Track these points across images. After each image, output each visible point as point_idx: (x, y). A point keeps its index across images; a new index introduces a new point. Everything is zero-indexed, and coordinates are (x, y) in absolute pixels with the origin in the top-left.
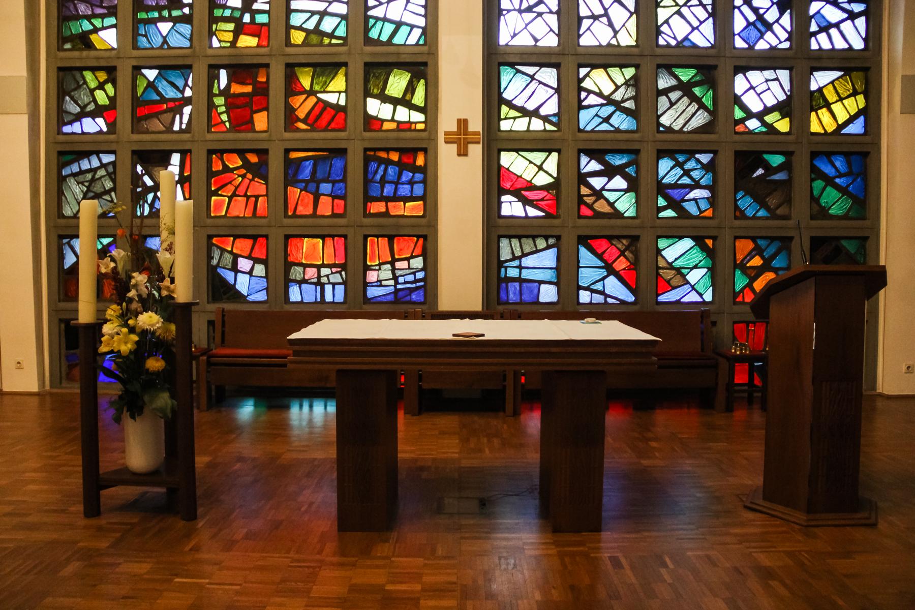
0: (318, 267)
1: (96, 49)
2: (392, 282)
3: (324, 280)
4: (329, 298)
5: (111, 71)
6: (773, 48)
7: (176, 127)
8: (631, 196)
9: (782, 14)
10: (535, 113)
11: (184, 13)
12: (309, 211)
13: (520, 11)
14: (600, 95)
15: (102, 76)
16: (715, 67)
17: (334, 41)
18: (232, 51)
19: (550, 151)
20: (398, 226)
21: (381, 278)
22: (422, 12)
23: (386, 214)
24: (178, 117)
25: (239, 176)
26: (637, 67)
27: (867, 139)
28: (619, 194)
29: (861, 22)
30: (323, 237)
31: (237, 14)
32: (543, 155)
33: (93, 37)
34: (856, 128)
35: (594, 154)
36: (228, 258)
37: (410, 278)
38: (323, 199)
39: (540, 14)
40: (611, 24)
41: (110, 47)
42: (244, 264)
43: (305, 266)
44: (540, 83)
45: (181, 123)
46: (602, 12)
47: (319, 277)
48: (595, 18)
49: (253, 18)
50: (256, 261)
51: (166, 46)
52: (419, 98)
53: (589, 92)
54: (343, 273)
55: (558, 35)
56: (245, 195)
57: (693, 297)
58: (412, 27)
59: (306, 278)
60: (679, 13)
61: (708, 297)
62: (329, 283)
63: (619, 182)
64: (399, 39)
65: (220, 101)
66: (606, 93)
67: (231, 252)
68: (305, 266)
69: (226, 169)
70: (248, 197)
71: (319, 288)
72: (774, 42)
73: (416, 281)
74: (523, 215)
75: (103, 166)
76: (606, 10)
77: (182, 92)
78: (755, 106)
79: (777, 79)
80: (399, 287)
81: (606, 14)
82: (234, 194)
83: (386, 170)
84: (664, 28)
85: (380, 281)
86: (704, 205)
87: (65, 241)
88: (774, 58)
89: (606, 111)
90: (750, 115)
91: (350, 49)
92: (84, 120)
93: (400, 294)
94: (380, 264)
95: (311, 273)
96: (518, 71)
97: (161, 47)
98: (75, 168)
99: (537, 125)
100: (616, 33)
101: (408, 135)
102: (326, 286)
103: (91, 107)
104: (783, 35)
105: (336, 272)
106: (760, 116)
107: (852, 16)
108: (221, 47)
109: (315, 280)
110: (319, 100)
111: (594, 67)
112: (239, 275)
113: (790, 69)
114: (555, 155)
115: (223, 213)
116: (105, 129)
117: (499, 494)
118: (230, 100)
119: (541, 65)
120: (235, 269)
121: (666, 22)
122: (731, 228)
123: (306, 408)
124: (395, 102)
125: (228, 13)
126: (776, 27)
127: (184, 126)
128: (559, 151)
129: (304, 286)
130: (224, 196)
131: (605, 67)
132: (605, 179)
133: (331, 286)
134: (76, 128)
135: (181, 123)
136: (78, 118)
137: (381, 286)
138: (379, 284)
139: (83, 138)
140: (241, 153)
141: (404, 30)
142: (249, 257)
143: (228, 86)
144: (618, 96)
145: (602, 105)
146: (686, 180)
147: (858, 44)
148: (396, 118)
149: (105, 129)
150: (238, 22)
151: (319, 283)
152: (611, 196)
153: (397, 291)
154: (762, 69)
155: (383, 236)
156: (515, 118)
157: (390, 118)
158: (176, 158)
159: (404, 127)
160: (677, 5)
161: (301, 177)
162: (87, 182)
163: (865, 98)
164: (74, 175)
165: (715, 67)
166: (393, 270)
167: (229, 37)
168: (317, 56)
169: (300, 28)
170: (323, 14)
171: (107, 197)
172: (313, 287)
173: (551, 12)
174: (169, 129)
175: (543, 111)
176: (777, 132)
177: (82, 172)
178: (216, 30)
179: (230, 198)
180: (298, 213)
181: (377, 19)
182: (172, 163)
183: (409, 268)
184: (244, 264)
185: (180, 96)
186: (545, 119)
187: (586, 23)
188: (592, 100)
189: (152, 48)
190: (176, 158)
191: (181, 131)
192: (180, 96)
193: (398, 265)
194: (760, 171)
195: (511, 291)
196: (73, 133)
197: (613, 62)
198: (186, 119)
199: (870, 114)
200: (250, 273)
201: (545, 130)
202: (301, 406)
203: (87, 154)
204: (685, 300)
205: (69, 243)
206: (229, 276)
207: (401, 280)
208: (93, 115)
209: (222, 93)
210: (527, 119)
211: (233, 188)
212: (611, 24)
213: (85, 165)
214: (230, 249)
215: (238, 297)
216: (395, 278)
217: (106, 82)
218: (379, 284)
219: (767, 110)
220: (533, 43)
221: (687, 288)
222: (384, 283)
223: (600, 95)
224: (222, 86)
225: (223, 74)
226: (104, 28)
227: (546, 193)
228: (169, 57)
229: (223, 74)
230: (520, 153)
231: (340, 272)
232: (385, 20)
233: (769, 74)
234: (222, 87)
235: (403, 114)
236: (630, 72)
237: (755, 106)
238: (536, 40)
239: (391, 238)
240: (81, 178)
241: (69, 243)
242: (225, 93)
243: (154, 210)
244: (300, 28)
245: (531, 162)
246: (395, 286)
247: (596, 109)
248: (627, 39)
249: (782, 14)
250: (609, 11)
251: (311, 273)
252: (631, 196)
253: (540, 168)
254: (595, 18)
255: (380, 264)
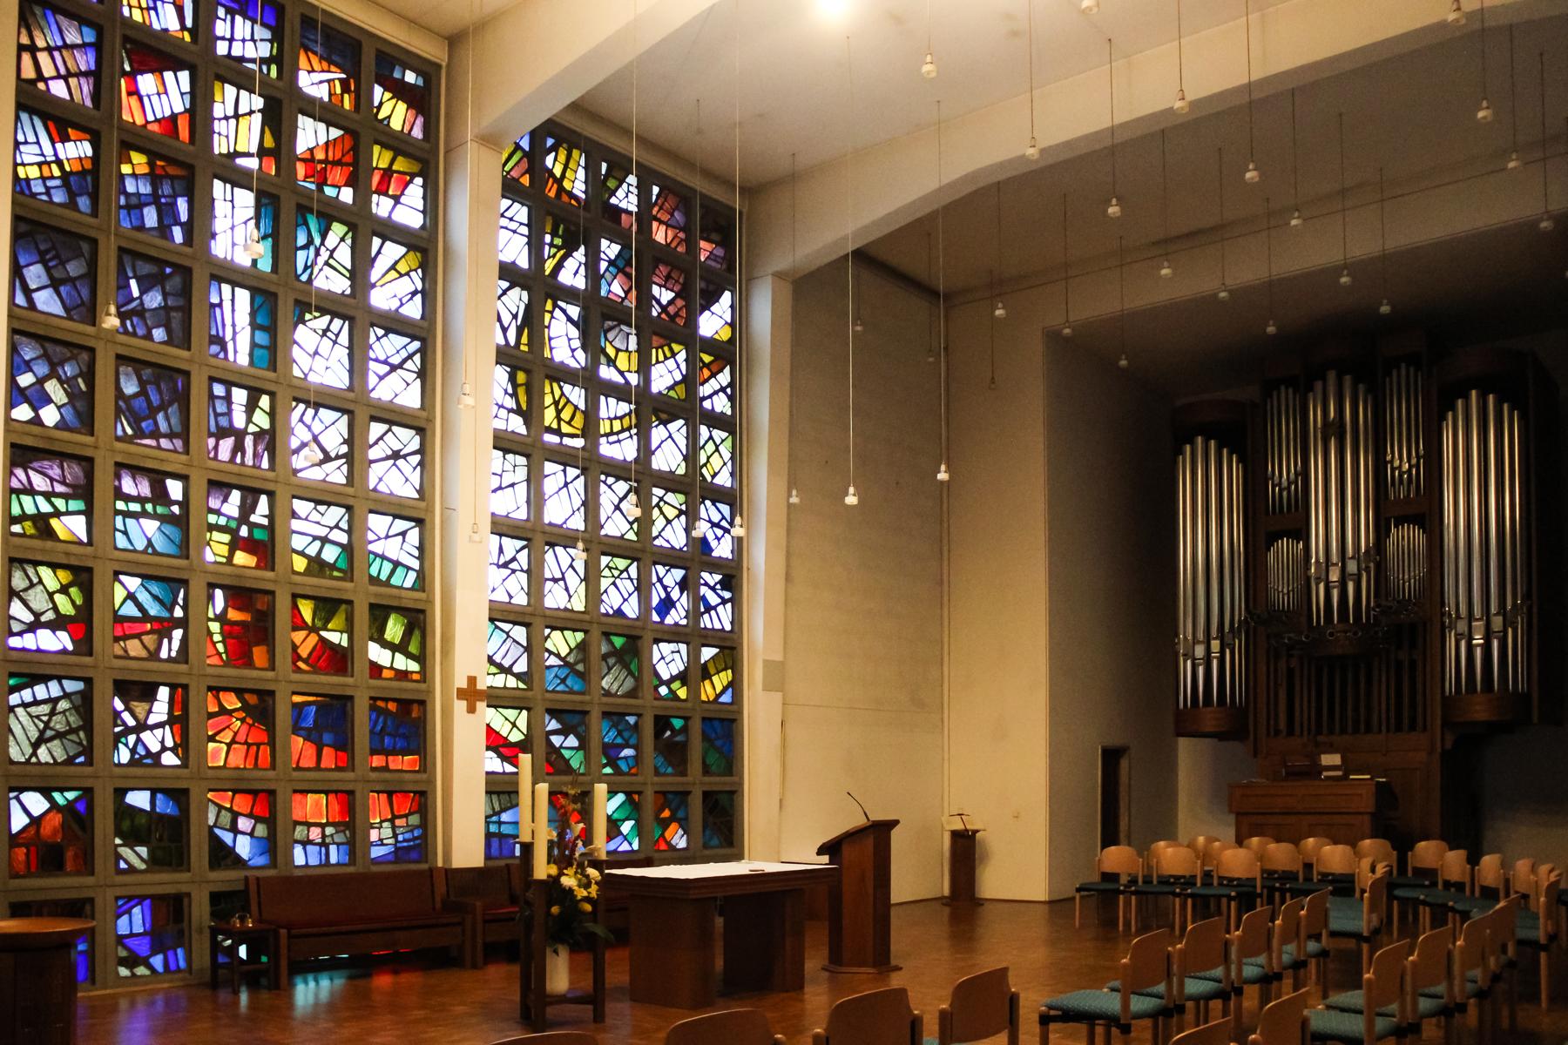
0: (323, 826)
1: (59, 540)
2: (391, 841)
3: (328, 840)
4: (333, 859)
5: (77, 571)
6: (676, 624)
7: (164, 654)
8: (580, 754)
9: (682, 593)
10: (507, 671)
11: (173, 513)
12: (312, 764)
13: (499, 566)
14: (558, 656)
15: (64, 576)
16: (639, 637)
17: (336, 574)
18: (228, 569)
19: (521, 709)
20: (401, 781)
21: (382, 837)
22: (416, 553)
23: (386, 769)
24: (166, 641)
25: (237, 719)
26: (586, 632)
27: (734, 708)
28: (573, 752)
29: (729, 606)
30: (327, 793)
31: (233, 524)
32: (516, 712)
33: (54, 522)
34: (726, 698)
35: (553, 713)
36: (226, 818)
37: (408, 836)
38: (326, 751)
39: (514, 571)
40: (567, 589)
41: (75, 539)
42: (244, 824)
43: (309, 825)
44: (514, 641)
45: (170, 650)
46: (560, 576)
47: (324, 836)
48: (555, 580)
49: (250, 532)
50: (258, 820)
51: (150, 550)
52: (413, 648)
53: (551, 653)
54: (347, 832)
55: (527, 594)
56: (246, 743)
57: (625, 847)
58: (409, 568)
59: (311, 838)
60: (614, 584)
61: (636, 846)
62: (334, 843)
63: (572, 741)
64: (395, 581)
65: (215, 627)
66: (563, 655)
67: (230, 810)
68: (309, 825)
69: (223, 711)
70: (249, 745)
71: (323, 849)
72: (677, 619)
73: (415, 838)
74: (501, 771)
75: (66, 696)
76: (563, 574)
77: (171, 610)
78: (665, 676)
79: (678, 652)
80: (399, 845)
81: (563, 579)
82: (233, 741)
83: (385, 722)
84: (604, 597)
85: (381, 840)
86: (631, 762)
87: (12, 795)
88: (678, 634)
89: (566, 671)
90: (662, 682)
91: (355, 587)
92: (39, 632)
93: (400, 853)
94: (382, 822)
95: (315, 834)
96: (497, 627)
97: (145, 552)
98: (27, 695)
99: (512, 682)
100: (570, 597)
101: (405, 684)
102: (331, 846)
103: (50, 616)
104: (683, 614)
105: (341, 831)
106: (668, 683)
107: (724, 602)
108: (216, 562)
109: (320, 841)
110: (323, 640)
111: (554, 628)
112: (240, 837)
113: (688, 644)
114: (525, 713)
115: (222, 764)
116: (70, 647)
117: (552, 392)
118: (226, 627)
119: (515, 623)
120: (235, 830)
121: (606, 591)
122: (652, 784)
123: (312, 984)
124: (394, 648)
125: (222, 521)
126: (678, 605)
127: (173, 654)
128: (528, 709)
129: (309, 848)
130: (221, 742)
131: (562, 629)
132: (562, 738)
133: (335, 846)
134: (28, 641)
135: (170, 650)
136: (32, 628)
137: (383, 845)
138: (381, 843)
139: (38, 656)
140: (239, 692)
141: (400, 571)
142: (249, 816)
143: (225, 611)
144: (571, 659)
145: (559, 666)
146: (619, 740)
147: (728, 627)
148: (395, 666)
149: (70, 647)
150: (234, 533)
151: (324, 844)
152: (567, 754)
153: (397, 849)
154: (669, 642)
155: (383, 792)
156: (494, 674)
157: (389, 666)
158: (163, 693)
159: (403, 675)
160: (613, 576)
161: (303, 725)
162: (45, 715)
163: (733, 672)
164: (25, 705)
165: (639, 637)
166: (394, 828)
167: (224, 550)
168: (150, 354)
169: (302, 553)
170: (325, 540)
171: (73, 737)
172: (318, 848)
173: (522, 570)
174: (154, 655)
175: (516, 669)
176: (677, 698)
177: (36, 703)
178: (210, 539)
179: (229, 745)
180: (301, 765)
181: (376, 555)
182: (158, 698)
183: (408, 825)
184: (244, 824)
185: (165, 614)
186: (518, 676)
187: (549, 585)
188: (553, 661)
189: (135, 551)
190: (163, 693)
191: (170, 660)
192: (165, 614)
193: (398, 822)
194: (668, 733)
195: (139, 945)
196: (24, 649)
197: (569, 626)
198: (176, 644)
199: (735, 685)
200: (251, 834)
201: (518, 688)
202: (306, 983)
203: (44, 679)
204: (620, 849)
205: (17, 798)
206: (227, 837)
207: (400, 838)
208: (54, 626)
209: (217, 618)
210: (504, 675)
211: (232, 734)
212: (567, 589)
213: (41, 691)
214: (228, 806)
215: (238, 861)
216: (395, 836)
217: (71, 585)
218: (381, 843)
219: (673, 679)
220: (506, 599)
221: (619, 839)
222: (385, 842)
223: (558, 656)
224: (218, 611)
225: (219, 594)
226: (68, 513)
227: (603, 280)
228: (148, 564)
229: (219, 594)
230: (500, 709)
231: (344, 832)
232: (383, 557)
233: (673, 646)
234: (218, 612)
235: (401, 662)
236: (580, 636)
237: (665, 676)
238: (511, 597)
239: (390, 794)
240: (33, 710)
241: (17, 798)
242: (220, 618)
243: (137, 756)
244: (302, 553)
245: (507, 719)
246: (395, 845)
247: (556, 669)
248: (579, 604)
249: (682, 593)
250: (566, 575)
251: (315, 834)
252: (580, 754)
253: (514, 725)
254: (555, 580)
255: (382, 822)
